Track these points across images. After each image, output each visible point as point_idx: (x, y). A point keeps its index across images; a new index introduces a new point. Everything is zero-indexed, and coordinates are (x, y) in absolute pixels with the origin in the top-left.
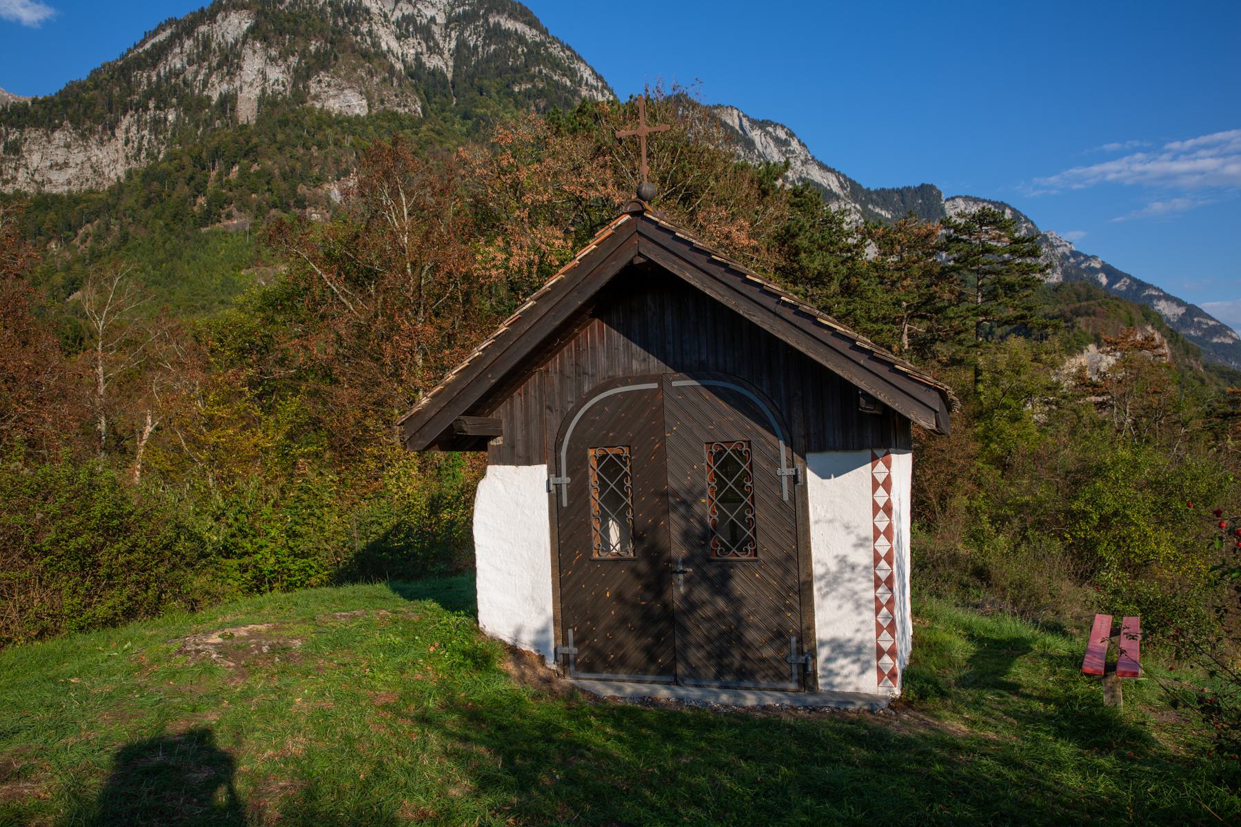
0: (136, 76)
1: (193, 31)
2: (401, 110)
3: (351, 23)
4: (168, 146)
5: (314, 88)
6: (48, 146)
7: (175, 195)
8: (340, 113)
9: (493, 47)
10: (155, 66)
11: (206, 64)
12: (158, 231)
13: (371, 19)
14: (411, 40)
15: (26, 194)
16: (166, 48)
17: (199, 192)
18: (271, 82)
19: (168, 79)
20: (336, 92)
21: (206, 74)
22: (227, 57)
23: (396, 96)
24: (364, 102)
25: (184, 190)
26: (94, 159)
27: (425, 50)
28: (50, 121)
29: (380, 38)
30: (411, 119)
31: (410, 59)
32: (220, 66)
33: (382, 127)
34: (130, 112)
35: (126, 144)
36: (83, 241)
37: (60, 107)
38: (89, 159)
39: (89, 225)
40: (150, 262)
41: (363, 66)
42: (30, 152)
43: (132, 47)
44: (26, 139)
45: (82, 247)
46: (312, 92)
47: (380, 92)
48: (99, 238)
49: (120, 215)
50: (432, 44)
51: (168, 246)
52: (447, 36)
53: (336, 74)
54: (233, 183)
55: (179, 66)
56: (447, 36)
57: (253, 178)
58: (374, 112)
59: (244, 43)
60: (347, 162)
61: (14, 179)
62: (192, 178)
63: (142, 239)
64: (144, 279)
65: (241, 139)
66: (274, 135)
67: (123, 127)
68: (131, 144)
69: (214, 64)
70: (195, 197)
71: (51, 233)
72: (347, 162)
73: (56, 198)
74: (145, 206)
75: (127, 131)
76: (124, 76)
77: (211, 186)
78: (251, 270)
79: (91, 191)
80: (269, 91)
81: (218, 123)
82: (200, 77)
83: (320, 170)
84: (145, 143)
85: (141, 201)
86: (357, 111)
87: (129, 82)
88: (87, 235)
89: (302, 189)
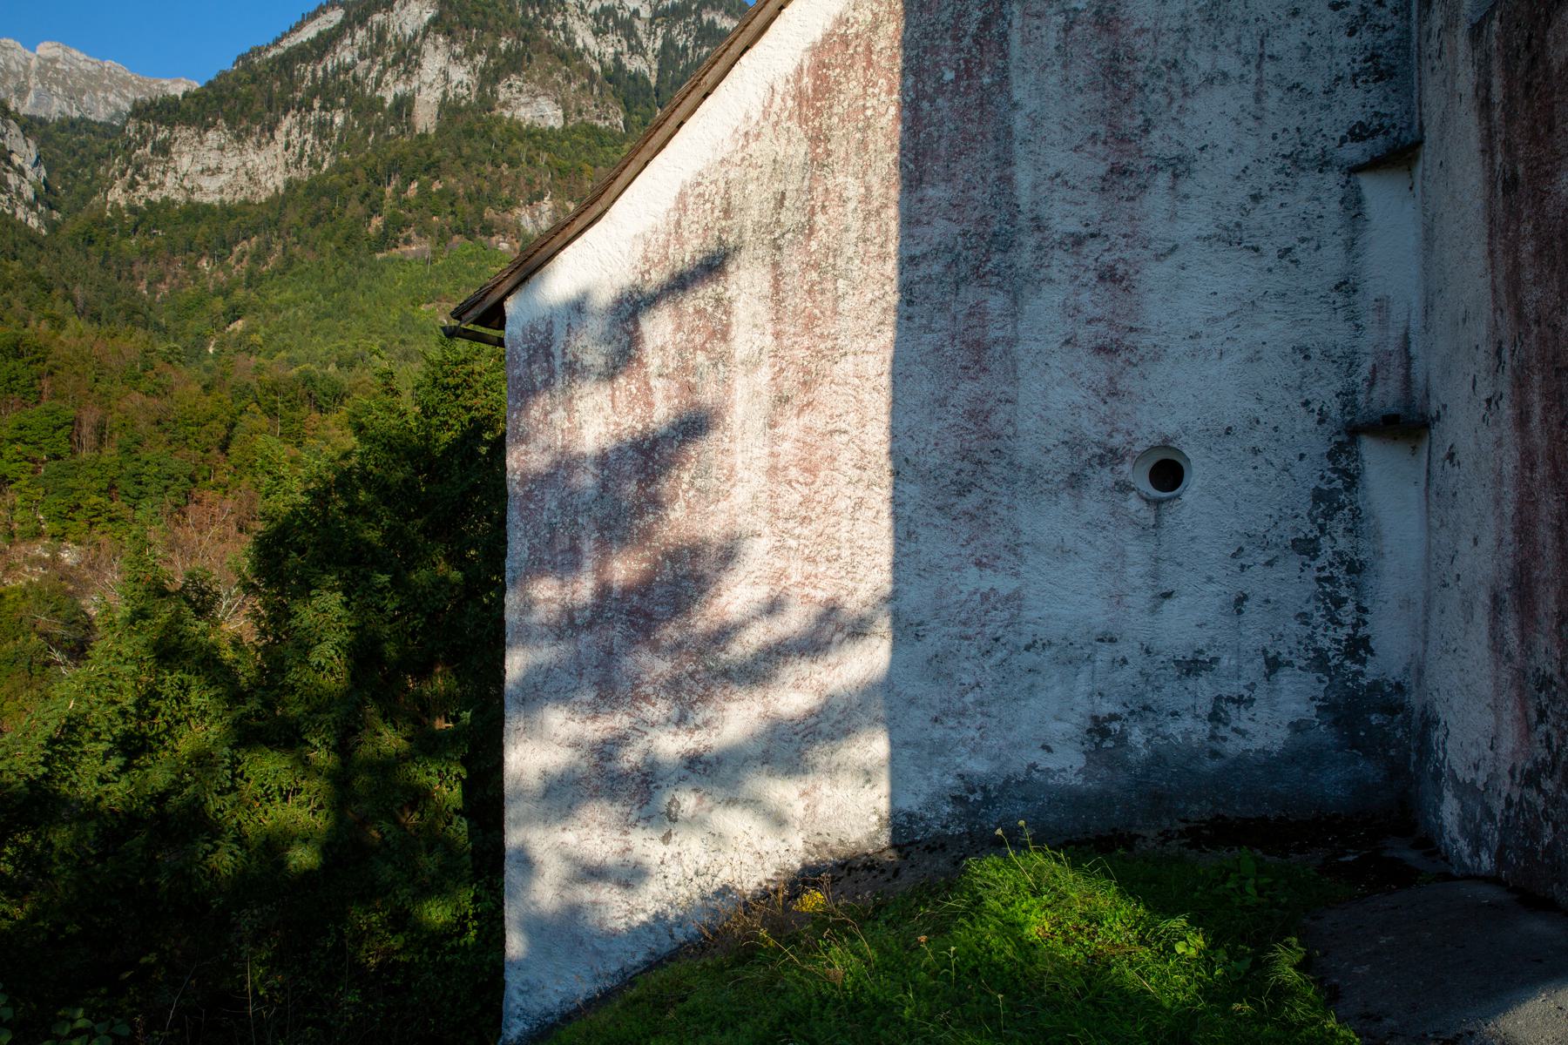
0: (299, 70)
1: (366, 19)
2: (601, 124)
3: (542, 14)
4: (333, 154)
5: (503, 93)
6: (199, 147)
7: (348, 214)
8: (532, 125)
9: (705, 50)
10: (320, 58)
11: (380, 59)
12: (328, 255)
13: (566, 10)
14: (611, 37)
15: (174, 202)
16: (334, 39)
17: (375, 212)
18: (454, 84)
19: (335, 74)
20: (528, 100)
21: (380, 71)
22: (404, 52)
23: (596, 106)
24: (560, 113)
25: (355, 209)
26: (250, 165)
27: (626, 49)
28: (203, 119)
29: (575, 34)
30: (612, 134)
31: (608, 59)
32: (395, 62)
33: (580, 143)
34: (293, 112)
35: (287, 148)
36: (239, 261)
37: (215, 102)
38: (244, 164)
39: (245, 242)
40: (319, 290)
41: (559, 70)
42: (180, 153)
43: (287, 30)
44: (176, 139)
45: (238, 267)
46: (501, 97)
47: (578, 100)
48: (258, 257)
49: (283, 233)
50: (634, 42)
51: (340, 273)
52: (652, 34)
53: (529, 78)
54: (414, 203)
55: (348, 60)
56: (652, 34)
57: (435, 198)
58: (570, 124)
59: (425, 36)
60: (541, 183)
61: (162, 184)
62: (367, 195)
63: (310, 263)
64: (315, 310)
65: (422, 151)
66: (459, 148)
67: (284, 129)
68: (291, 149)
69: (389, 60)
70: (370, 217)
71: (202, 249)
72: (541, 183)
73: (208, 208)
74: (313, 225)
75: (288, 134)
76: (286, 69)
77: (388, 203)
78: (432, 306)
79: (246, 203)
80: (451, 95)
81: (392, 130)
82: (373, 74)
83: (511, 191)
84: (308, 148)
85: (308, 218)
86: (551, 123)
87: (291, 76)
88: (244, 253)
89: (489, 213)
